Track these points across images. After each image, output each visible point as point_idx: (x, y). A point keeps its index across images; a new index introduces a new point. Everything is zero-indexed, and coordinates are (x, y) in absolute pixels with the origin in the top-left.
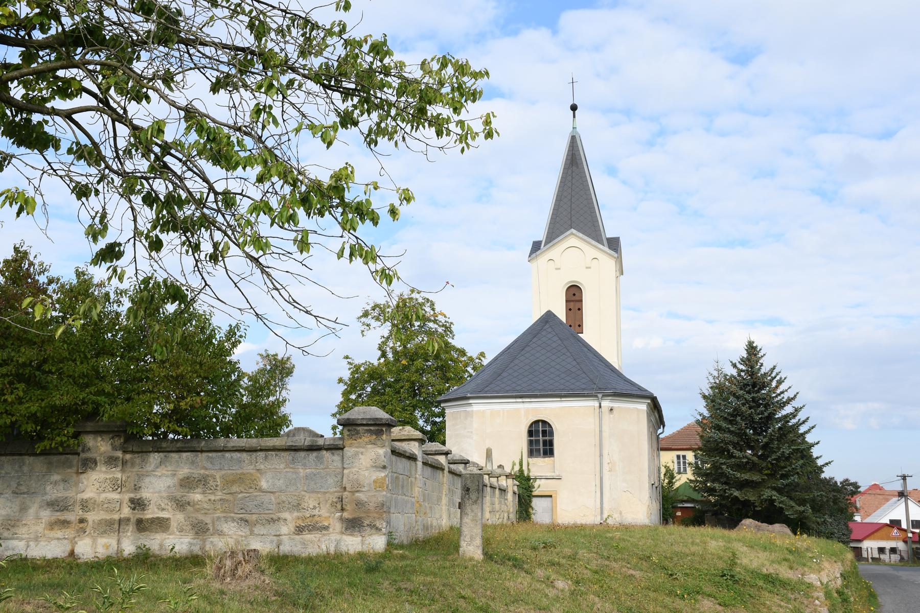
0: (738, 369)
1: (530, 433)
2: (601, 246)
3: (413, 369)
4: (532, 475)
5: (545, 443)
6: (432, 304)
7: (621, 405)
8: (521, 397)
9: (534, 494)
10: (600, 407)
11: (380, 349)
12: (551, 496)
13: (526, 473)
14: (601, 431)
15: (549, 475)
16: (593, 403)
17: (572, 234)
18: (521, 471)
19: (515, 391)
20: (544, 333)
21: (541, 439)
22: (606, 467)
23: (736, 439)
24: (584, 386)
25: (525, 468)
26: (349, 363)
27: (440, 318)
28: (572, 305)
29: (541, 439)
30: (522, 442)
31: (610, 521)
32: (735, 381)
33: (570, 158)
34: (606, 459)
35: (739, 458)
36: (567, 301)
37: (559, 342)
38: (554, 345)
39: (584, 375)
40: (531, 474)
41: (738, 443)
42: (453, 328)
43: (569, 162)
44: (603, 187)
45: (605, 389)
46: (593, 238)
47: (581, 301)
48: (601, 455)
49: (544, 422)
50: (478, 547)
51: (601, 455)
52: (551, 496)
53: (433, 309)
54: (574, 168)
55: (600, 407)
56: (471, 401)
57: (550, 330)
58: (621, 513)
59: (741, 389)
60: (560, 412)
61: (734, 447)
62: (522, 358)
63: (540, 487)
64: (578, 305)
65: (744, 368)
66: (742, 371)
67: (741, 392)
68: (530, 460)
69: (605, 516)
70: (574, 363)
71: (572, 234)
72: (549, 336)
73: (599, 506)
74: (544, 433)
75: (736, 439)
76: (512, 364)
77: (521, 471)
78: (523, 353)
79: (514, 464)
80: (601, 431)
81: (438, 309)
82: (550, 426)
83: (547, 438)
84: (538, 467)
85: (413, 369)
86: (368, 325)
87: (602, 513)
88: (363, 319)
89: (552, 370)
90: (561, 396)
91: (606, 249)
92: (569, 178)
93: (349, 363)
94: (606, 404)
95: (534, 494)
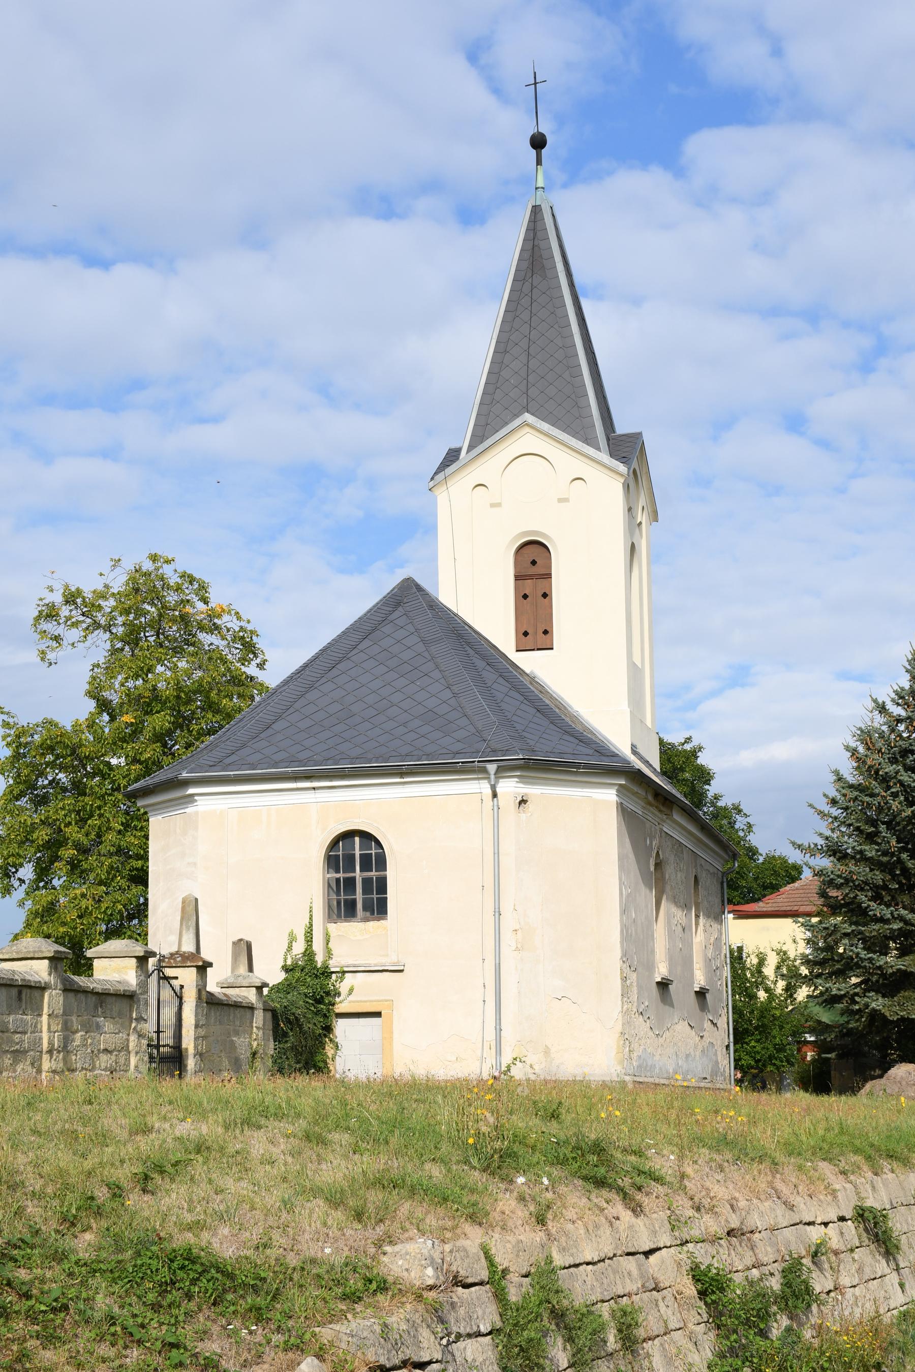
0: (890, 715)
1: (332, 861)
2: (591, 451)
3: (147, 733)
4: (334, 965)
5: (367, 882)
6: (202, 590)
7: (548, 795)
8: (308, 777)
9: (340, 1008)
10: (495, 795)
11: (91, 694)
12: (378, 1014)
13: (319, 959)
14: (497, 853)
15: (374, 962)
16: (474, 788)
17: (526, 424)
18: (309, 954)
19: (291, 762)
20: (387, 629)
21: (357, 876)
22: (508, 940)
23: (878, 877)
24: (458, 747)
25: (318, 946)
26: (6, 725)
27: (226, 621)
28: (528, 586)
29: (357, 876)
30: (311, 883)
31: (517, 1072)
32: (880, 744)
33: (527, 255)
34: (509, 921)
35: (882, 920)
36: (518, 578)
37: (420, 648)
38: (406, 655)
39: (464, 722)
40: (331, 963)
41: (885, 887)
42: (260, 643)
43: (525, 265)
44: (611, 333)
45: (506, 752)
46: (575, 435)
47: (549, 576)
48: (498, 913)
49: (366, 836)
50: (871, 1094)
51: (498, 913)
52: (378, 1014)
53: (205, 601)
54: (537, 279)
55: (495, 795)
56: (191, 791)
57: (402, 622)
58: (547, 1051)
59: (893, 761)
60: (403, 813)
61: (877, 898)
62: (330, 686)
63: (352, 993)
64: (541, 585)
65: (903, 713)
66: (899, 721)
67: (890, 769)
68: (332, 927)
69: (506, 1060)
70: (447, 694)
71: (526, 424)
72: (401, 634)
73: (491, 1035)
74: (366, 862)
75: (878, 877)
76: (303, 702)
77: (309, 954)
78: (335, 672)
79: (292, 939)
80: (497, 853)
81: (217, 598)
82: (379, 844)
83: (373, 874)
84: (351, 944)
85: (147, 733)
86: (57, 639)
87: (499, 1052)
88: (46, 626)
89: (394, 711)
90: (401, 772)
91: (605, 457)
92: (525, 301)
93: (6, 725)
94: (510, 787)
95: (340, 1008)
